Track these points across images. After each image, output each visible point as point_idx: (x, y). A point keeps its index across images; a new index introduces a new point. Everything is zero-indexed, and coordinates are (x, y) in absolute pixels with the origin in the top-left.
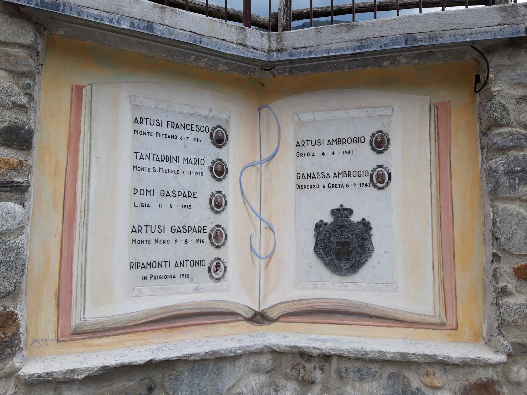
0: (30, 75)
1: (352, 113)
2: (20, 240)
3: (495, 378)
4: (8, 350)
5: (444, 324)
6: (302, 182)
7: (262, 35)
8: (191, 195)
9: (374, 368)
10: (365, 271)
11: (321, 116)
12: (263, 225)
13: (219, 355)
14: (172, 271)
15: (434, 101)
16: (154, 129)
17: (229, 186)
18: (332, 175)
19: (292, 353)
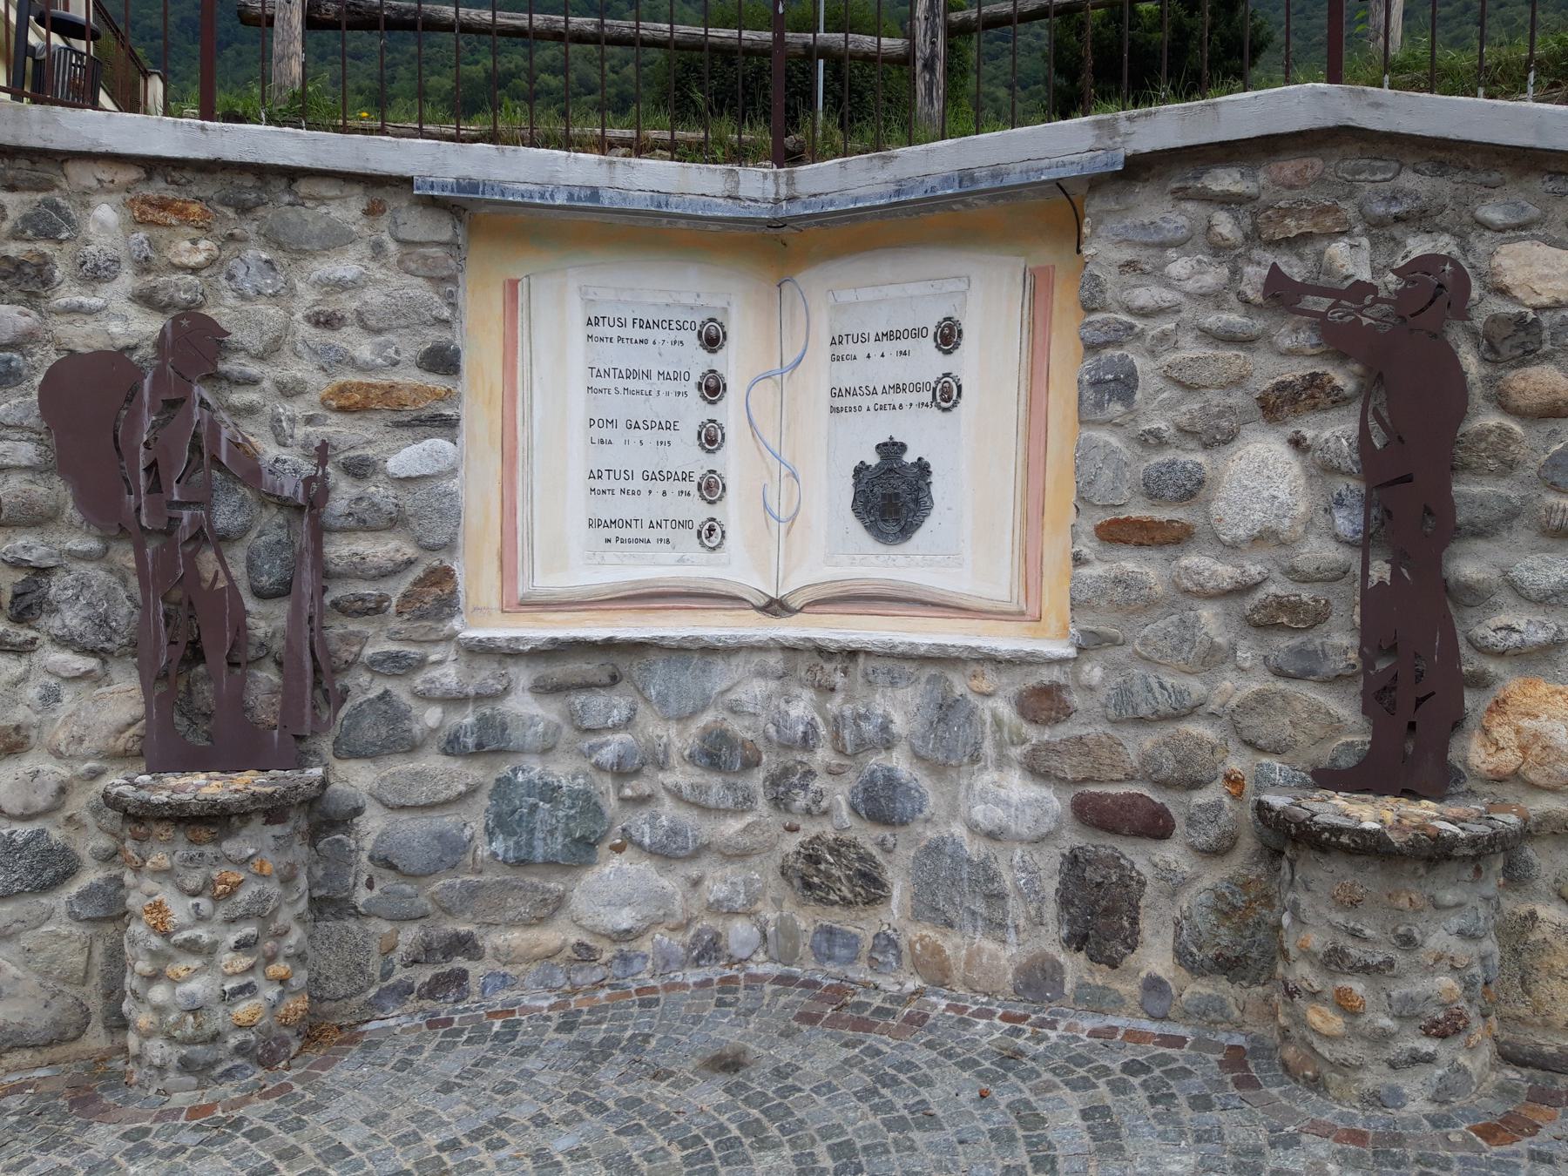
0: (452, 279)
1: (913, 289)
2: (453, 485)
3: (1063, 681)
4: (447, 610)
5: (1022, 613)
6: (839, 402)
7: (765, 176)
8: (670, 426)
9: (909, 667)
10: (919, 537)
11: (866, 294)
12: (785, 471)
13: (702, 644)
14: (645, 533)
15: (1031, 265)
16: (615, 332)
17: (729, 412)
18: (879, 390)
19: (808, 650)
